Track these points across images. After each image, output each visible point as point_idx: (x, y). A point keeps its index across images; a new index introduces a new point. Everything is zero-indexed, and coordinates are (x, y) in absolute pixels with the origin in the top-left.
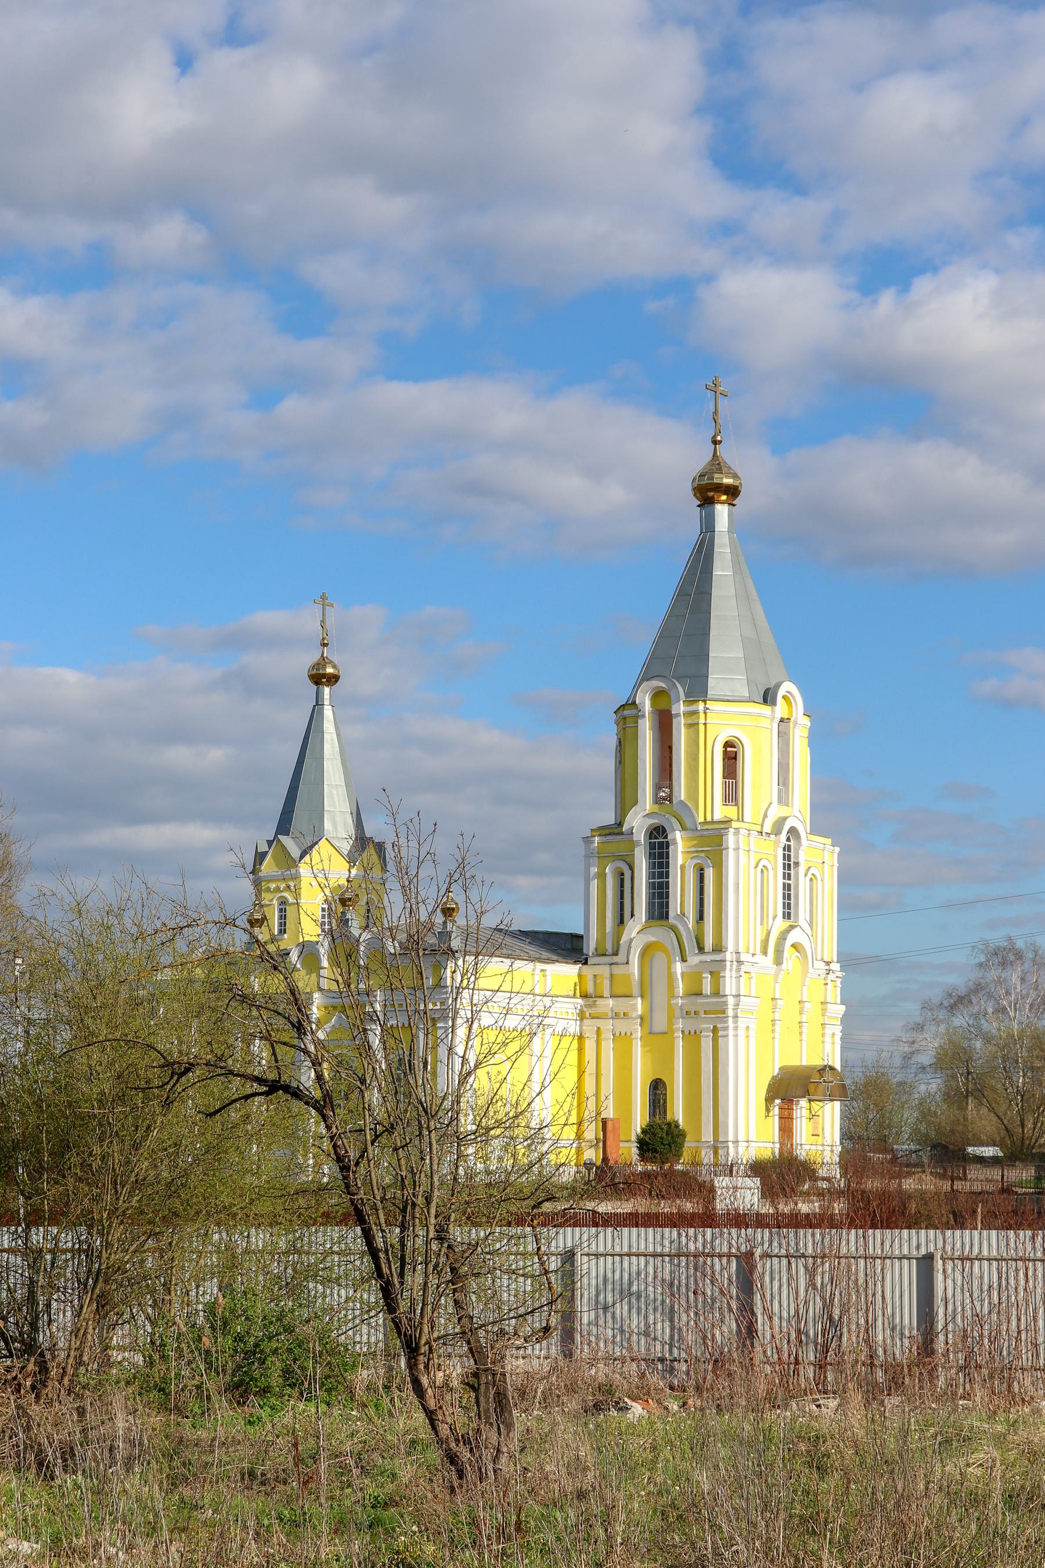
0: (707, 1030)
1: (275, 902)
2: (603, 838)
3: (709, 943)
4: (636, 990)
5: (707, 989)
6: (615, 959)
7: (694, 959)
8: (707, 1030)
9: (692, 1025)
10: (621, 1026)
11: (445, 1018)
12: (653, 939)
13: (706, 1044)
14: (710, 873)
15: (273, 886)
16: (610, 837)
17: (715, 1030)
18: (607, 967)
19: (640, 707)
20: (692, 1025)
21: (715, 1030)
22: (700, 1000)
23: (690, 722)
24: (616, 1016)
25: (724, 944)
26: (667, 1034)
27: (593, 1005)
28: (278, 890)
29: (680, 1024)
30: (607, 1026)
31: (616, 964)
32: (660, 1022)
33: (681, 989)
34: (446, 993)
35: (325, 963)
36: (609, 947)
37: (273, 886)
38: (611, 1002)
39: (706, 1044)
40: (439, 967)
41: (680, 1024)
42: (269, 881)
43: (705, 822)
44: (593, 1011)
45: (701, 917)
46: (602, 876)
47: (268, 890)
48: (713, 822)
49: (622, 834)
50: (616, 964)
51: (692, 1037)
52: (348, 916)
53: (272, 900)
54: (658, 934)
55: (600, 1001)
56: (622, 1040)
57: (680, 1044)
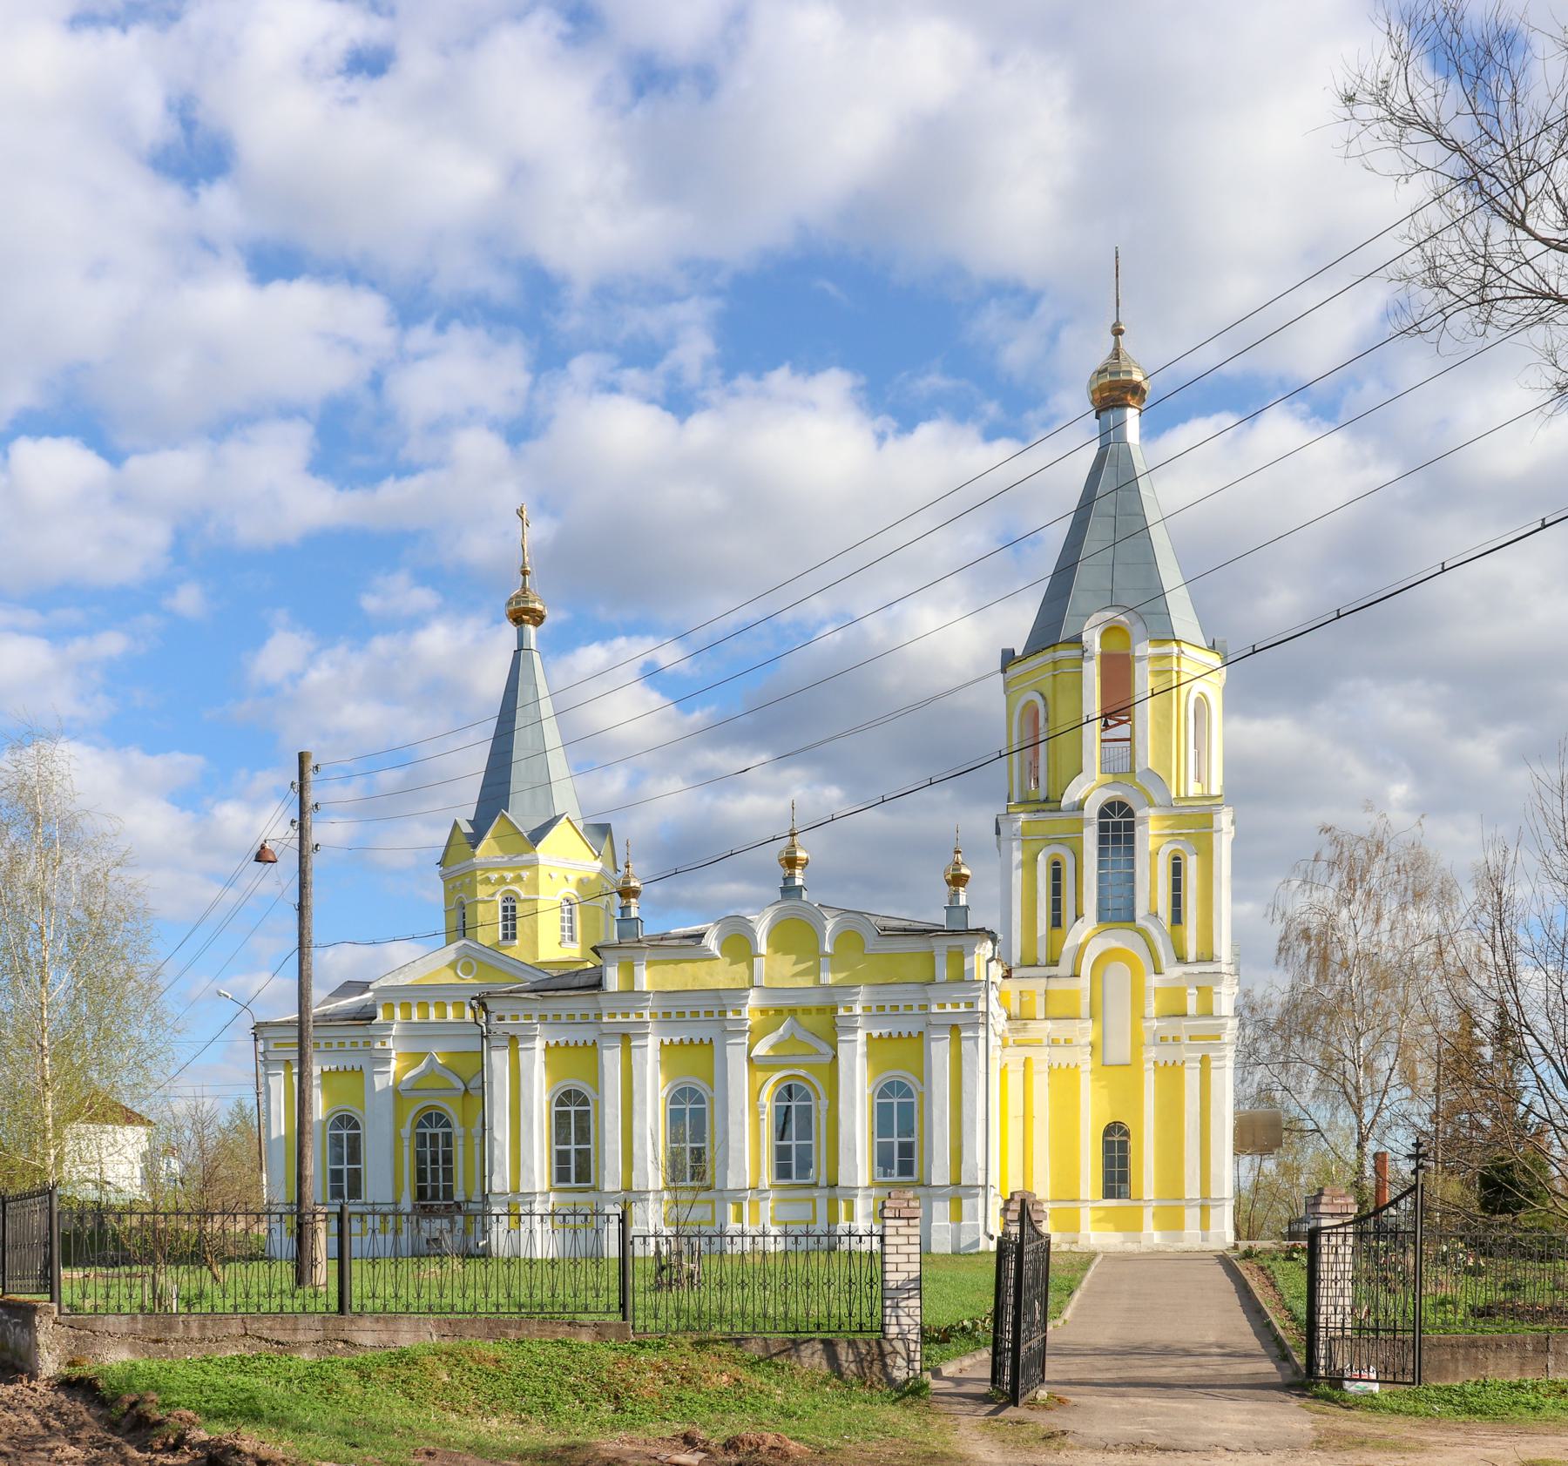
0: (1192, 1060)
1: (499, 898)
2: (1032, 816)
3: (1192, 952)
4: (1084, 1010)
5: (1192, 1006)
6: (1053, 970)
7: (1174, 972)
8: (1192, 1060)
9: (1169, 1053)
10: (1062, 1056)
11: (975, 1025)
12: (1114, 944)
13: (1192, 1078)
14: (1192, 865)
15: (494, 876)
16: (1041, 815)
17: (1204, 1060)
18: (1044, 980)
19: (1086, 646)
20: (1169, 1053)
21: (1204, 1060)
22: (1184, 1022)
23: (1158, 668)
24: (1054, 1043)
25: (1216, 952)
26: (1131, 1066)
27: (1024, 1028)
28: (502, 881)
29: (1151, 1053)
30: (1041, 1057)
31: (1056, 976)
32: (1120, 1049)
33: (1152, 1008)
34: (979, 989)
35: (763, 948)
36: (1042, 956)
37: (494, 876)
38: (1049, 1025)
39: (1192, 1078)
40: (959, 956)
41: (1151, 1053)
42: (487, 870)
43: (1179, 798)
44: (1020, 1037)
45: (1177, 918)
46: (1030, 864)
47: (487, 881)
48: (1187, 798)
49: (1059, 810)
50: (1056, 976)
51: (1171, 1072)
52: (634, 913)
53: (493, 895)
54: (1115, 940)
55: (1032, 1025)
56: (1063, 1077)
57: (1150, 1079)
